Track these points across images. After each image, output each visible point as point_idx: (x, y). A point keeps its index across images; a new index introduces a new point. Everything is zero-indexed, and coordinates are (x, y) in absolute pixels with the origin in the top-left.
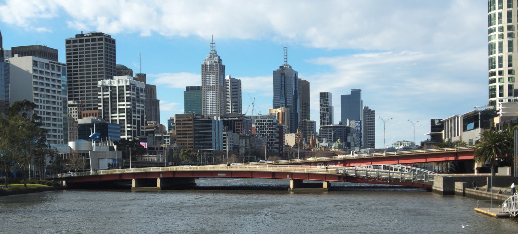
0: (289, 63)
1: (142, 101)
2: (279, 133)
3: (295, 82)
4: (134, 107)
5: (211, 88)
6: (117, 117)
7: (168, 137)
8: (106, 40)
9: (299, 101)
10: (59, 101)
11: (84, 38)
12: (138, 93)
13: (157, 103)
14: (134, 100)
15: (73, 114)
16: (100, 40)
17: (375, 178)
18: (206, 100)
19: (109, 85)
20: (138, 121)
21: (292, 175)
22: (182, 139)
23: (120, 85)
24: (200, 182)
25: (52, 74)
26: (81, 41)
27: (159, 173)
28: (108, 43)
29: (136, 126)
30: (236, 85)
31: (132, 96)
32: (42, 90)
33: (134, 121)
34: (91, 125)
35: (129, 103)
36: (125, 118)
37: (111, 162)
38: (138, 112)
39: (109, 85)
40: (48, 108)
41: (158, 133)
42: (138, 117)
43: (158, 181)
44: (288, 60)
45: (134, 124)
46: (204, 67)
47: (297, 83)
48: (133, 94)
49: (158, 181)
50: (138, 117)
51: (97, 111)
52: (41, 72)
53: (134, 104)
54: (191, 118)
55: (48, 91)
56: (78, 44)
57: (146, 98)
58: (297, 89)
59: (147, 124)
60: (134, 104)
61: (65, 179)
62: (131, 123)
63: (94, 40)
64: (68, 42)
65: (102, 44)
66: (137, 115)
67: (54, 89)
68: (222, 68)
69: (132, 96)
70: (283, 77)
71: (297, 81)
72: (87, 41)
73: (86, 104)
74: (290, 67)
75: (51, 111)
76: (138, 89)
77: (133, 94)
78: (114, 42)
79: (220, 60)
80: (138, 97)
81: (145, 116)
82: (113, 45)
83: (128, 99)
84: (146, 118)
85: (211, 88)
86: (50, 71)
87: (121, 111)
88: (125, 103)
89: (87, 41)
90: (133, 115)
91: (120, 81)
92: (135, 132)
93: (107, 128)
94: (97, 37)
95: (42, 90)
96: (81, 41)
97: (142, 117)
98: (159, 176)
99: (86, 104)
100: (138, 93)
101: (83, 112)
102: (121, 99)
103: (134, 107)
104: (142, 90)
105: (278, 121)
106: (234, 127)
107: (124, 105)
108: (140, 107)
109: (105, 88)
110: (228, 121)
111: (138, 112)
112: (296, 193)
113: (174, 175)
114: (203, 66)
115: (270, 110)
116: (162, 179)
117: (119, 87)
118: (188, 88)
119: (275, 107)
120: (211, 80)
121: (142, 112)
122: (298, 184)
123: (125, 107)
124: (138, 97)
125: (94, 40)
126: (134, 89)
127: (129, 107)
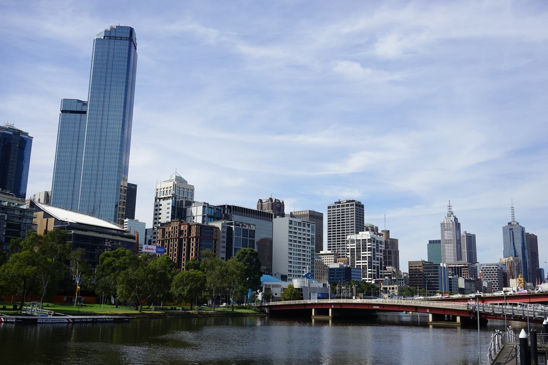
0: (517, 220)
1: (381, 251)
2: (504, 278)
3: (523, 236)
4: (374, 256)
5: (448, 242)
6: (361, 263)
7: (403, 280)
8: (356, 205)
9: (526, 251)
10: (309, 250)
11: (341, 205)
12: (377, 245)
13: (398, 251)
14: (374, 250)
15: (324, 261)
16: (352, 205)
17: (500, 315)
18: (444, 251)
19: (355, 239)
20: (378, 267)
21: (431, 309)
22: (414, 282)
23: (358, 239)
24: (390, 316)
25: (304, 230)
26: (338, 206)
27: (331, 304)
28: (358, 208)
29: (376, 270)
30: (471, 239)
31: (372, 247)
32: (295, 241)
33: (374, 266)
34: (337, 269)
35: (370, 252)
36: (367, 264)
37: (320, 295)
38: (378, 259)
39: (355, 239)
40: (299, 255)
41: (394, 276)
42: (377, 263)
43: (330, 310)
44: (515, 218)
45: (374, 268)
46: (443, 225)
47: (525, 237)
48: (373, 246)
49: (330, 310)
50: (377, 263)
51: (346, 259)
52: (295, 228)
53: (374, 253)
54: (421, 265)
55: (300, 242)
56: (336, 209)
57: (389, 250)
58: (525, 241)
59: (385, 269)
60: (374, 253)
61: (269, 306)
62: (371, 268)
63: (347, 205)
64: (329, 207)
65: (353, 208)
66: (376, 262)
67: (300, 240)
68: (458, 226)
69: (372, 247)
70: (511, 232)
71: (525, 235)
72: (343, 206)
73: (341, 253)
74: (518, 223)
75: (302, 257)
76: (377, 242)
77: (373, 246)
78: (363, 206)
79: (456, 219)
80: (377, 248)
81: (383, 263)
82: (361, 208)
83: (370, 249)
84: (384, 264)
85: (448, 242)
86: (302, 227)
87: (364, 258)
88: (367, 252)
89: (343, 206)
90: (373, 261)
91: (365, 235)
92: (374, 275)
93: (351, 271)
94: (350, 203)
95: (295, 241)
96: (338, 206)
97: (381, 263)
98: (331, 306)
99: (341, 253)
100: (377, 245)
101: (338, 259)
102: (364, 249)
103: (374, 256)
104: (381, 242)
105: (371, 254)
106: (461, 273)
107: (368, 254)
108: (380, 255)
109: (352, 241)
110: (455, 267)
111: (378, 259)
112: (435, 327)
113: (341, 306)
114: (441, 224)
115: (500, 259)
116: (333, 310)
117: (363, 240)
118: (430, 242)
119: (505, 257)
120: (450, 235)
121: (381, 259)
122: (437, 318)
123: (367, 255)
124: (377, 248)
125: (347, 206)
126: (374, 241)
127: (370, 255)
